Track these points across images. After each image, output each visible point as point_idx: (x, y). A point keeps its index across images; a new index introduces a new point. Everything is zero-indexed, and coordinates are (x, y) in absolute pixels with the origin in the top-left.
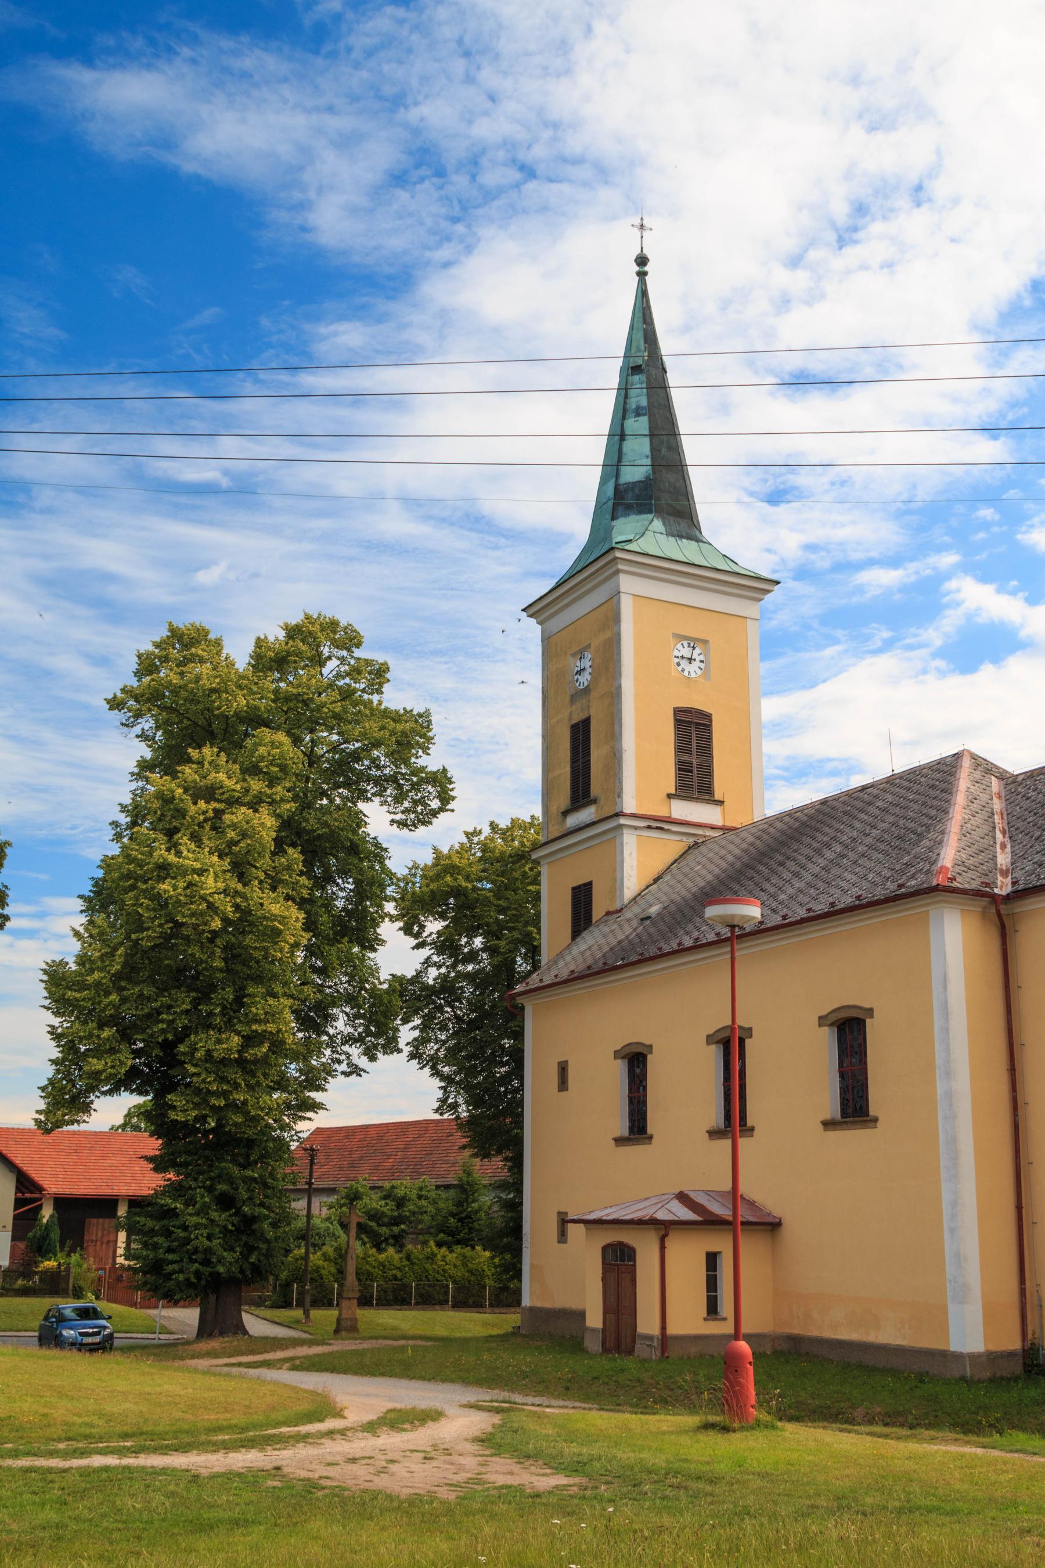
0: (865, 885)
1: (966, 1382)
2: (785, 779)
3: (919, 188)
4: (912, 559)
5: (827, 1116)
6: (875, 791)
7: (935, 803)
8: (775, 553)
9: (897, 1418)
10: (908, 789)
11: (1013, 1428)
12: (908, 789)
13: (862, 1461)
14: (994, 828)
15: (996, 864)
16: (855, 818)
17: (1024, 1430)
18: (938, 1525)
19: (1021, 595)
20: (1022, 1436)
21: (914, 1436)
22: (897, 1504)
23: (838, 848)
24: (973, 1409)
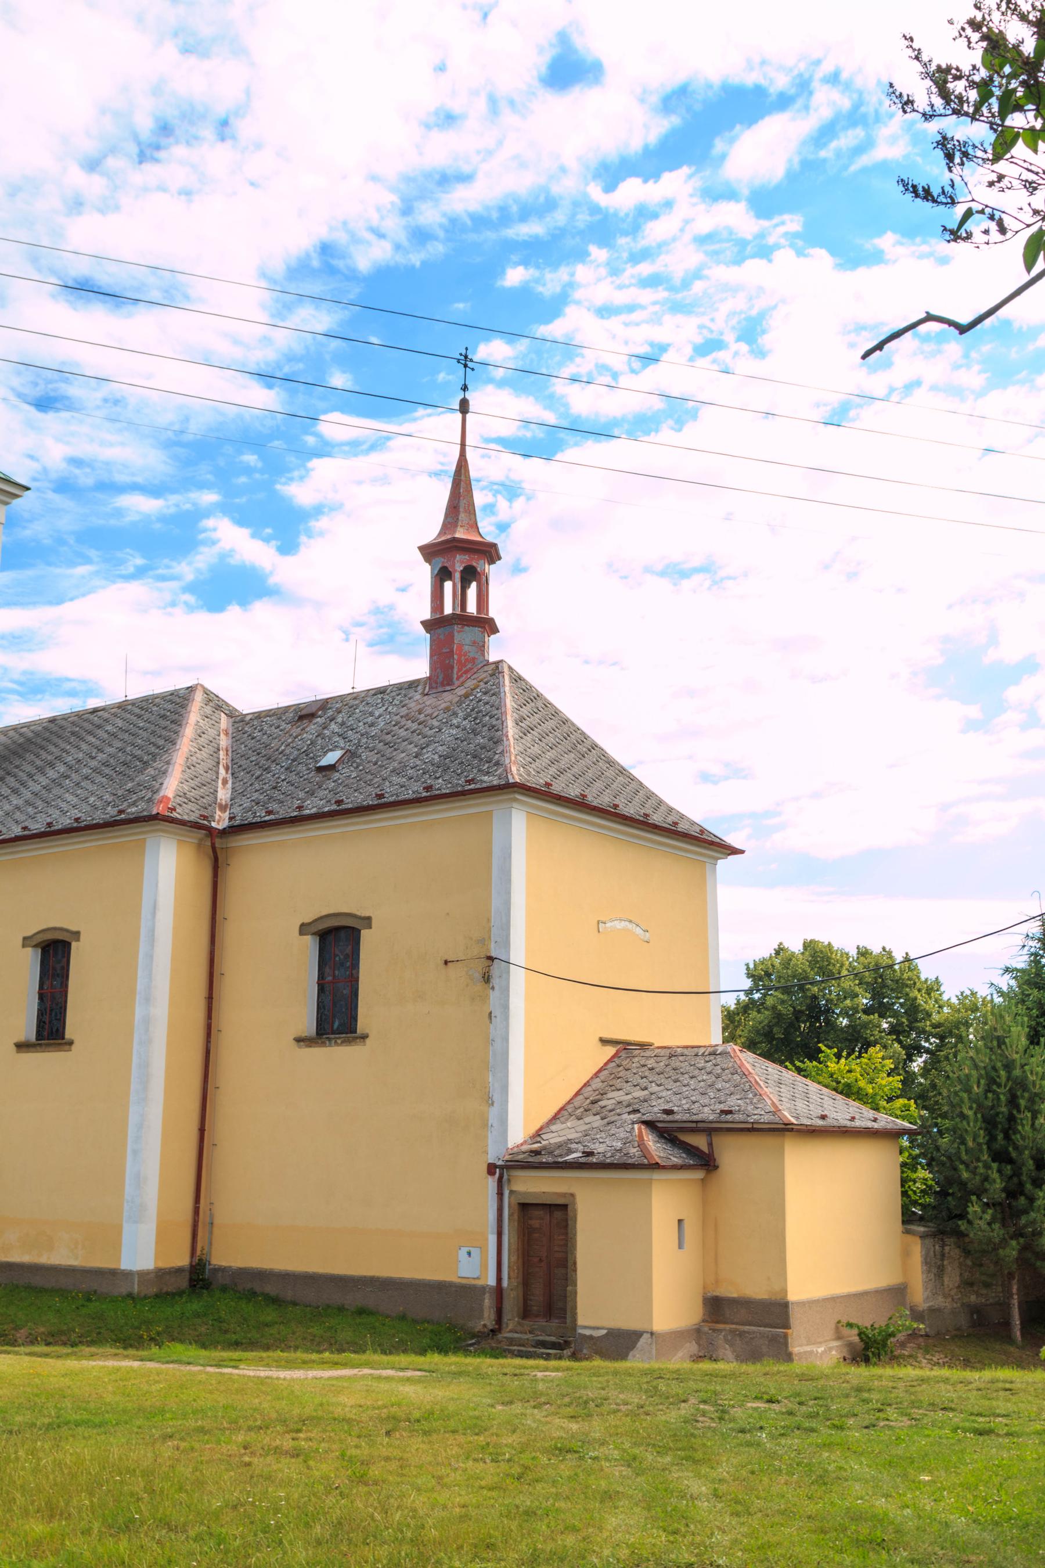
0: (85, 807)
1: (133, 1298)
2: (19, 694)
3: (225, 123)
4: (174, 491)
5: (21, 1037)
6: (106, 715)
7: (164, 733)
8: (37, 460)
9: (62, 1338)
10: (139, 716)
11: (173, 1340)
12: (139, 716)
13: (16, 1381)
14: (218, 763)
15: (216, 798)
16: (82, 739)
17: (182, 1341)
18: (84, 1438)
19: (274, 543)
20: (179, 1347)
21: (74, 1354)
22: (47, 1421)
23: (62, 769)
24: (136, 1324)
